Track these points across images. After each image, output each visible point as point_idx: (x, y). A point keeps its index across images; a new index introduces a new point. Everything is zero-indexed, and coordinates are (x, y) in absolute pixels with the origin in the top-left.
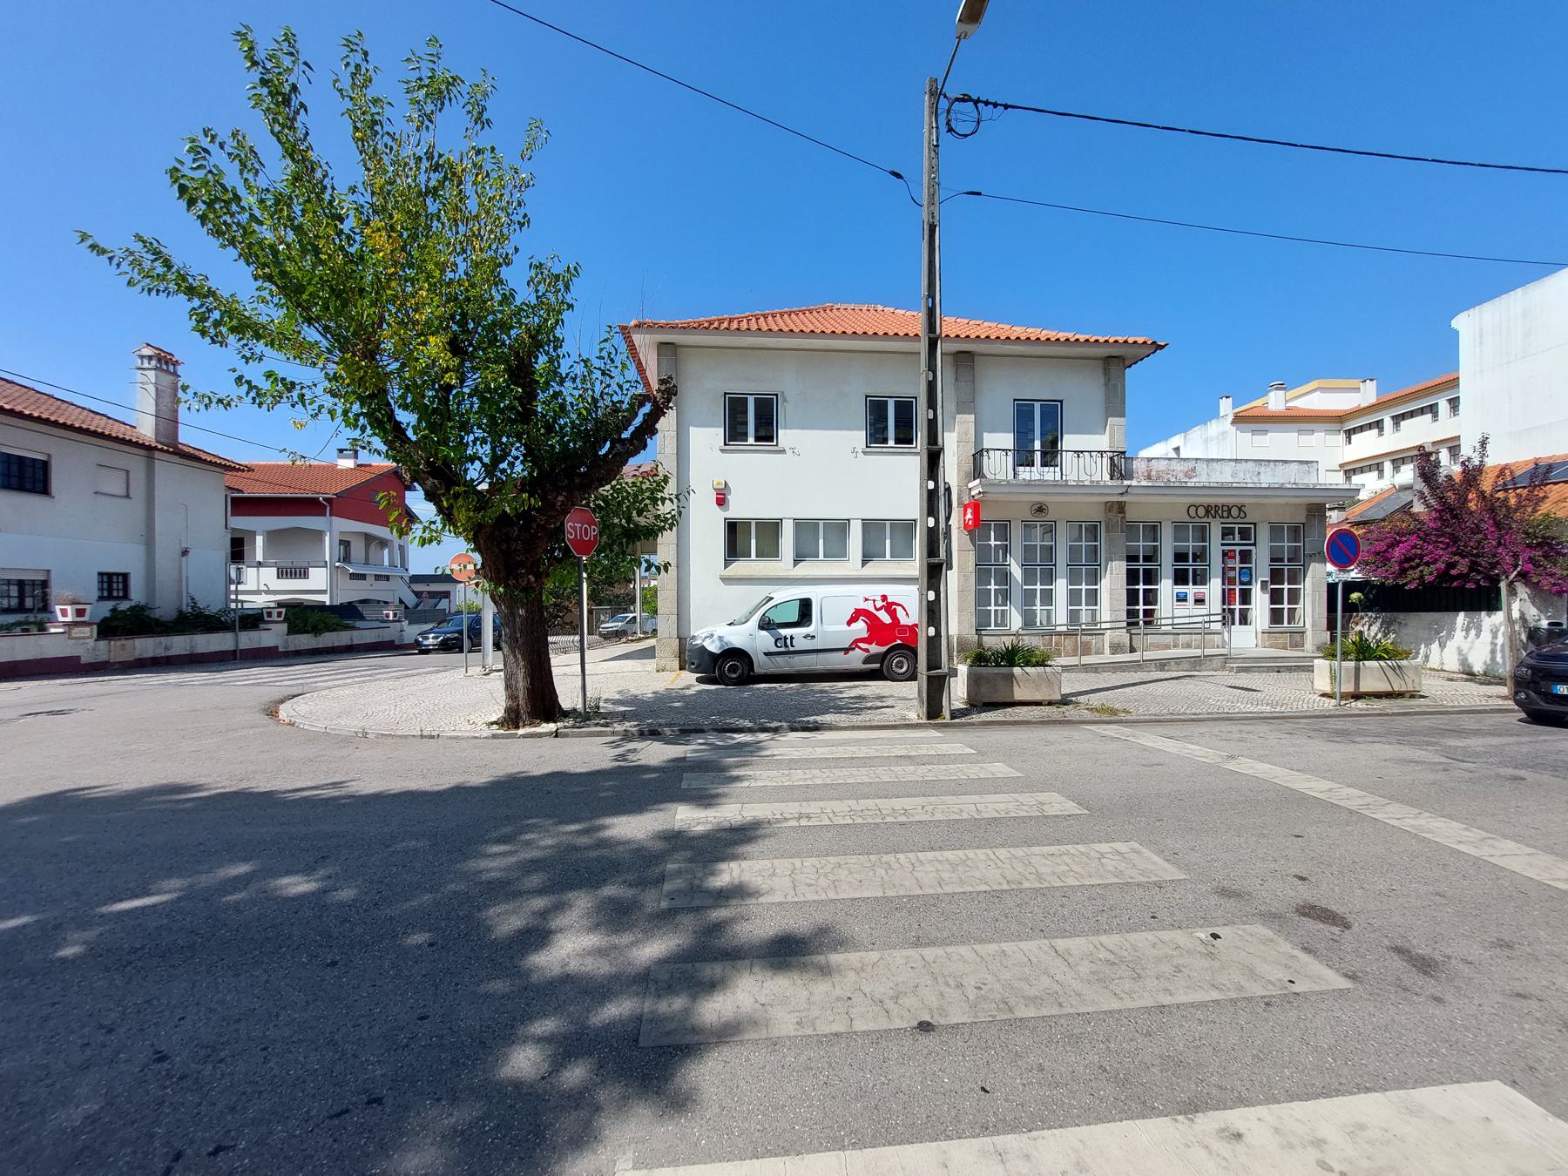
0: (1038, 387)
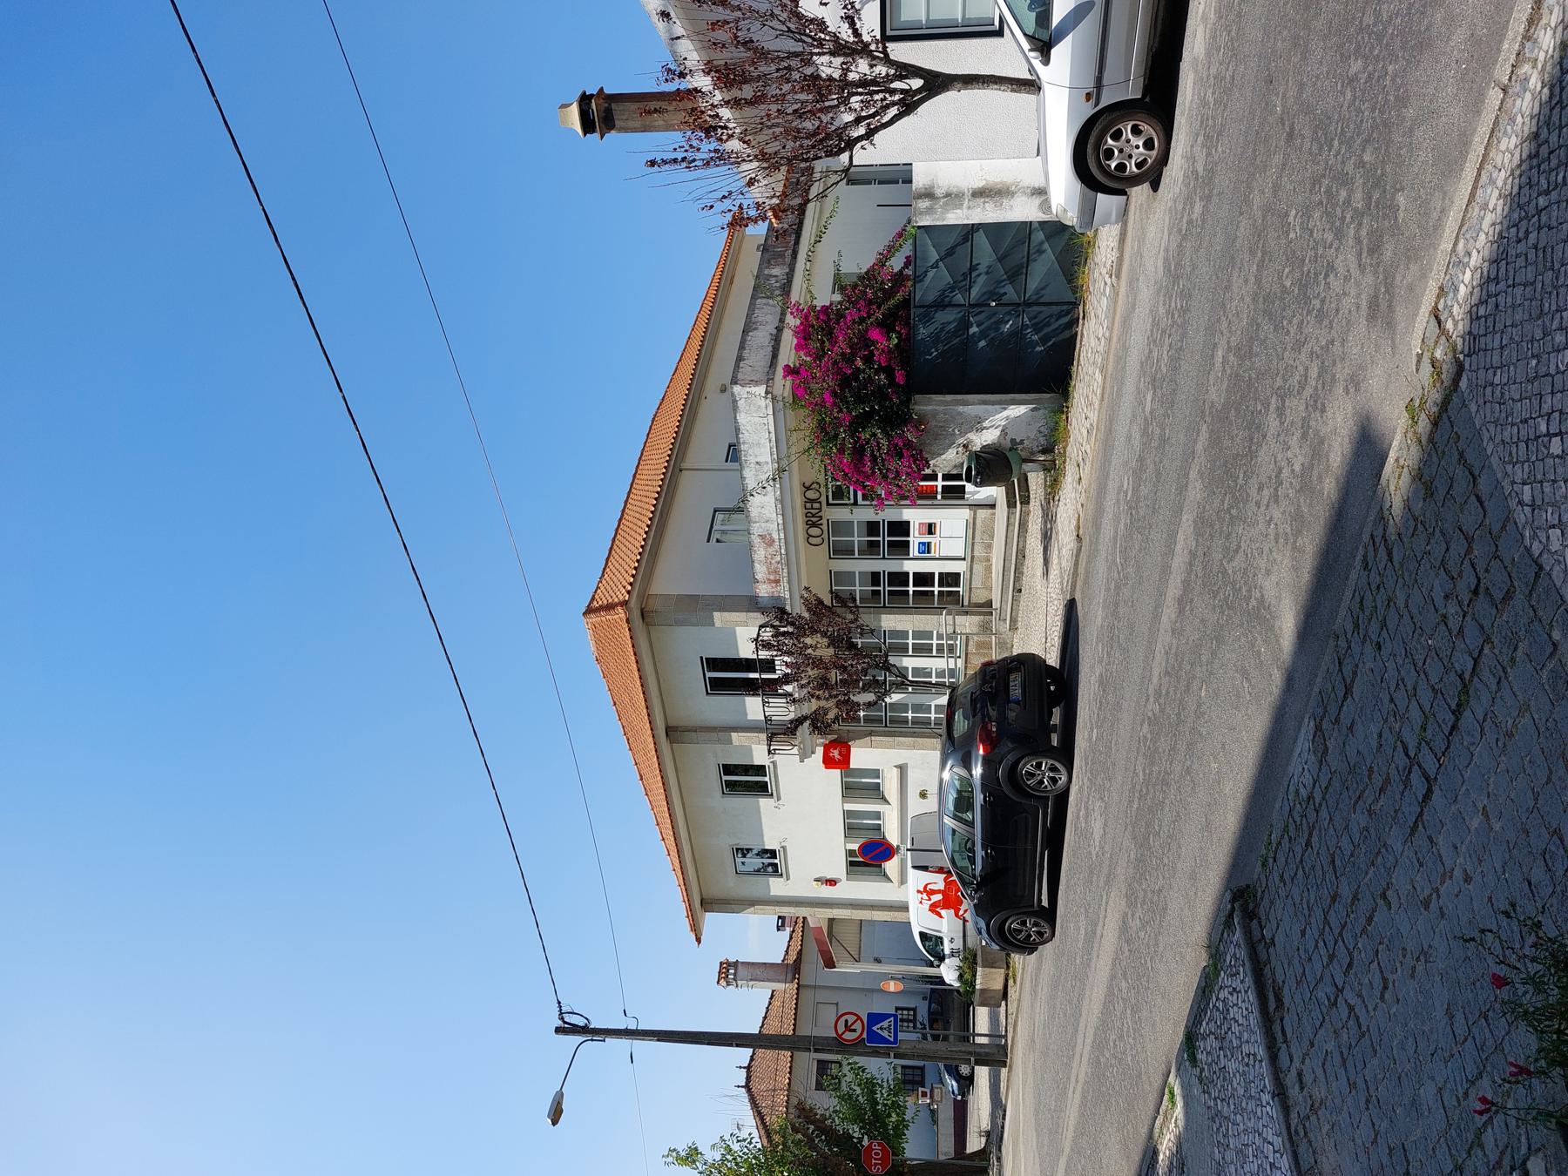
0: (695, 678)
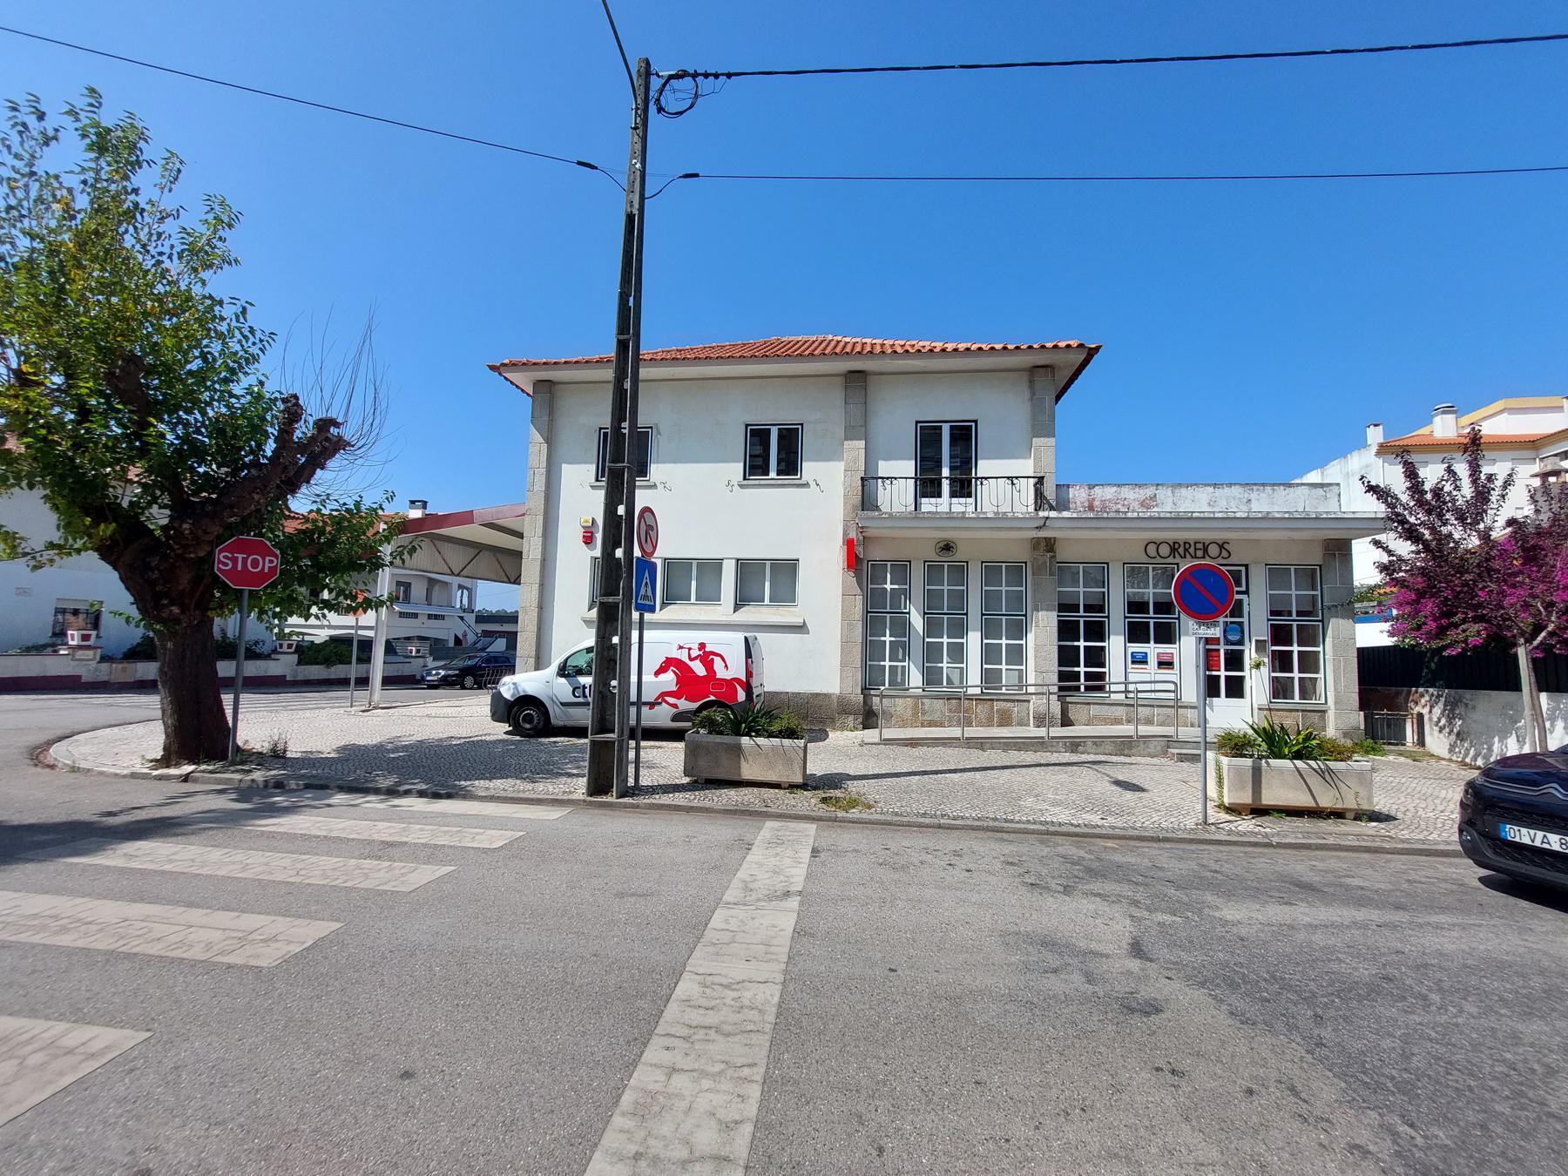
0: (946, 408)
